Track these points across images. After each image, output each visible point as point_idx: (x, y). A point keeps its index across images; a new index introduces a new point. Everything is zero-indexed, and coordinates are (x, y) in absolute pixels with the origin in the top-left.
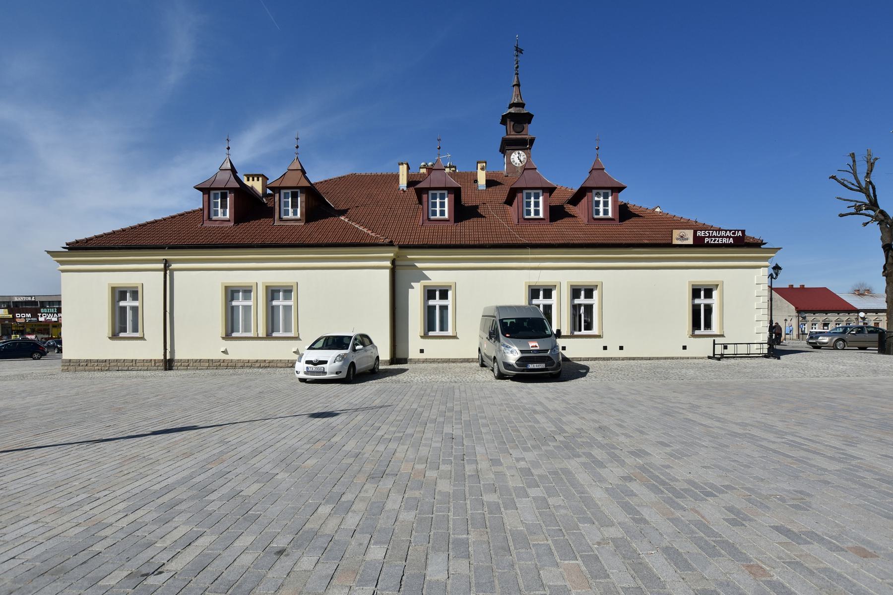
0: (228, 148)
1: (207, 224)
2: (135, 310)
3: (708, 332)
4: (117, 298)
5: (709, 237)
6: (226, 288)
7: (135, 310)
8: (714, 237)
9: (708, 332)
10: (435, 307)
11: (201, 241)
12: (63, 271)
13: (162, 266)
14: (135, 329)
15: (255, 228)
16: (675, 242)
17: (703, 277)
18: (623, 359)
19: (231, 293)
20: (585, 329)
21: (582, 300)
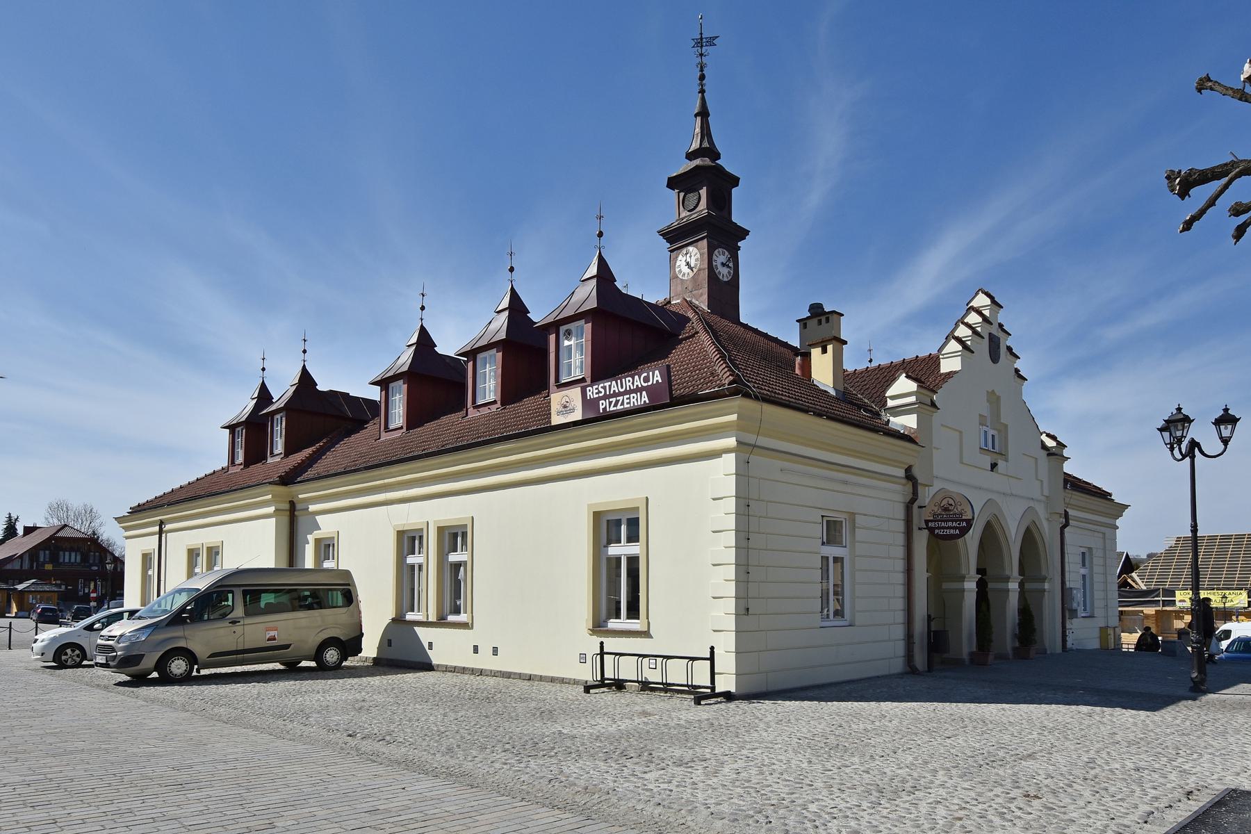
0: (512, 270)
1: (385, 437)
2: (633, 561)
3: (634, 625)
4: (604, 541)
5: (605, 397)
6: (597, 516)
7: (633, 561)
8: (615, 395)
9: (634, 625)
10: (618, 559)
11: (382, 459)
12: (127, 538)
13: (157, 529)
14: (633, 612)
15: (447, 426)
16: (556, 420)
17: (614, 492)
18: (495, 674)
19: (409, 541)
20: (629, 617)
21: (620, 550)
